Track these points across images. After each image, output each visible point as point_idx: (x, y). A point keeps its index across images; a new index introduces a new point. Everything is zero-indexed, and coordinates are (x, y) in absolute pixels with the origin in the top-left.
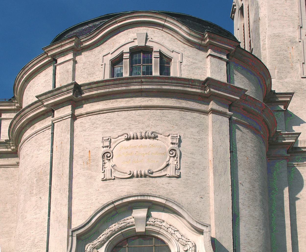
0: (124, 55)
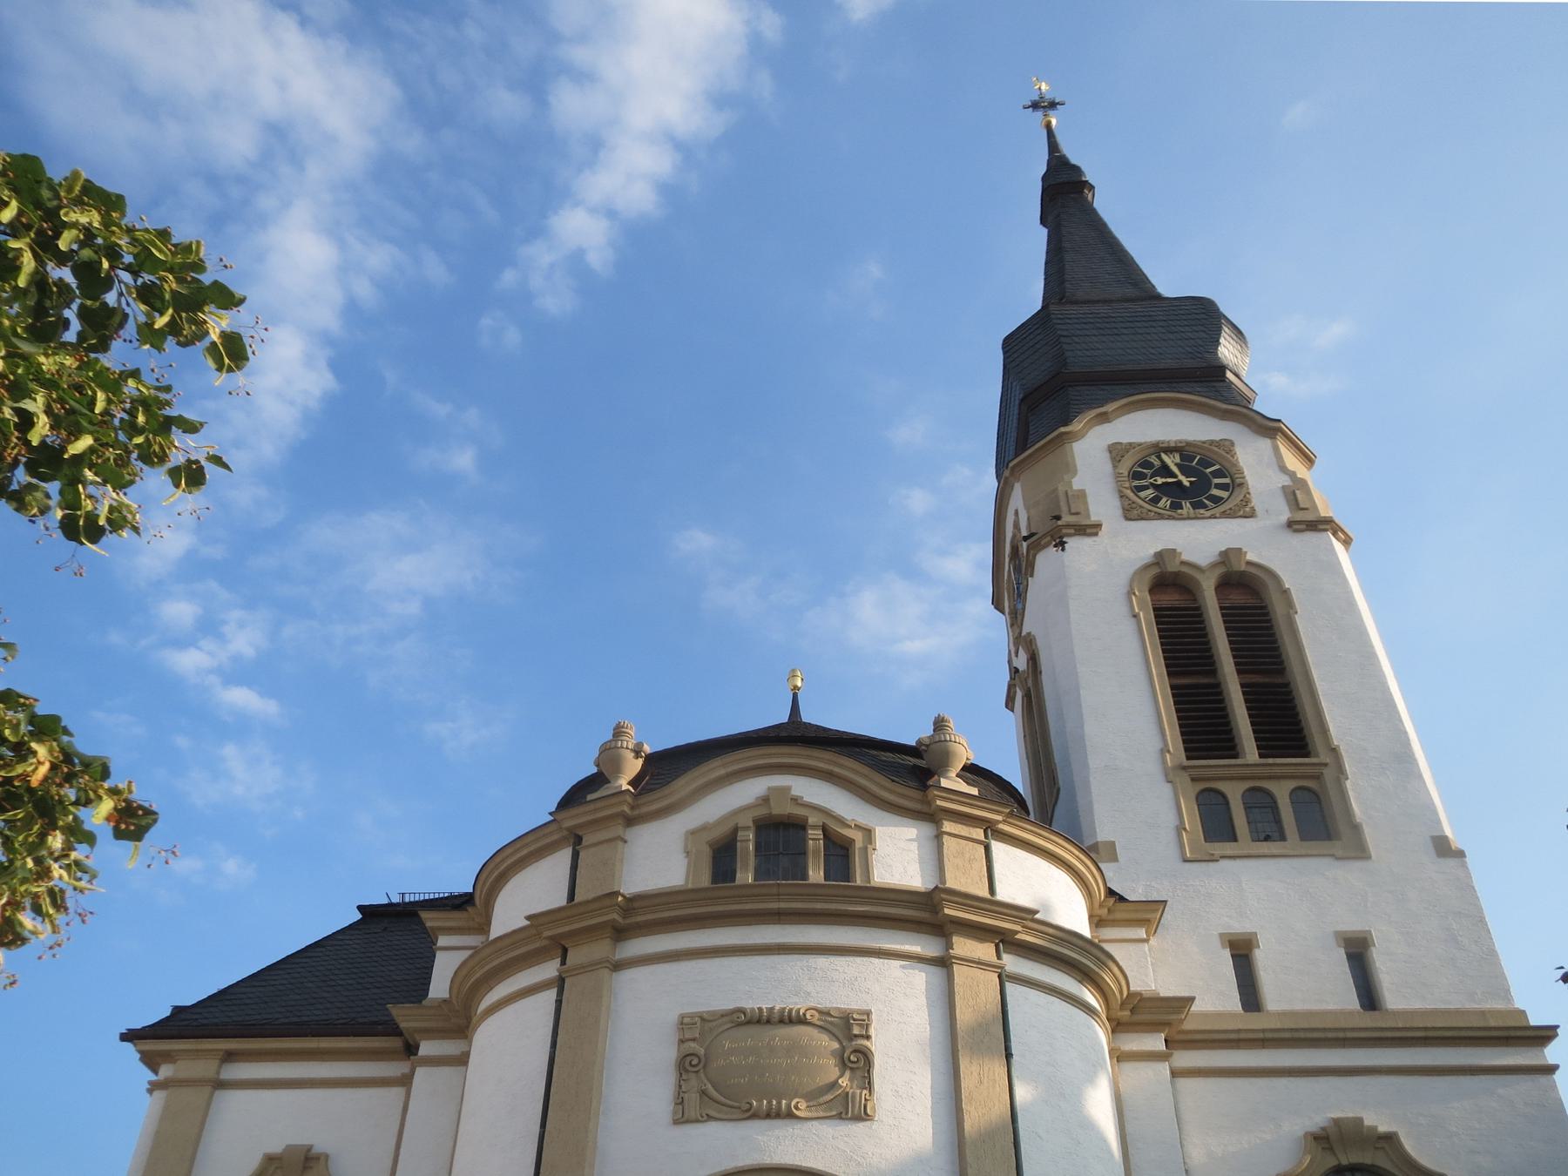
0: (740, 834)
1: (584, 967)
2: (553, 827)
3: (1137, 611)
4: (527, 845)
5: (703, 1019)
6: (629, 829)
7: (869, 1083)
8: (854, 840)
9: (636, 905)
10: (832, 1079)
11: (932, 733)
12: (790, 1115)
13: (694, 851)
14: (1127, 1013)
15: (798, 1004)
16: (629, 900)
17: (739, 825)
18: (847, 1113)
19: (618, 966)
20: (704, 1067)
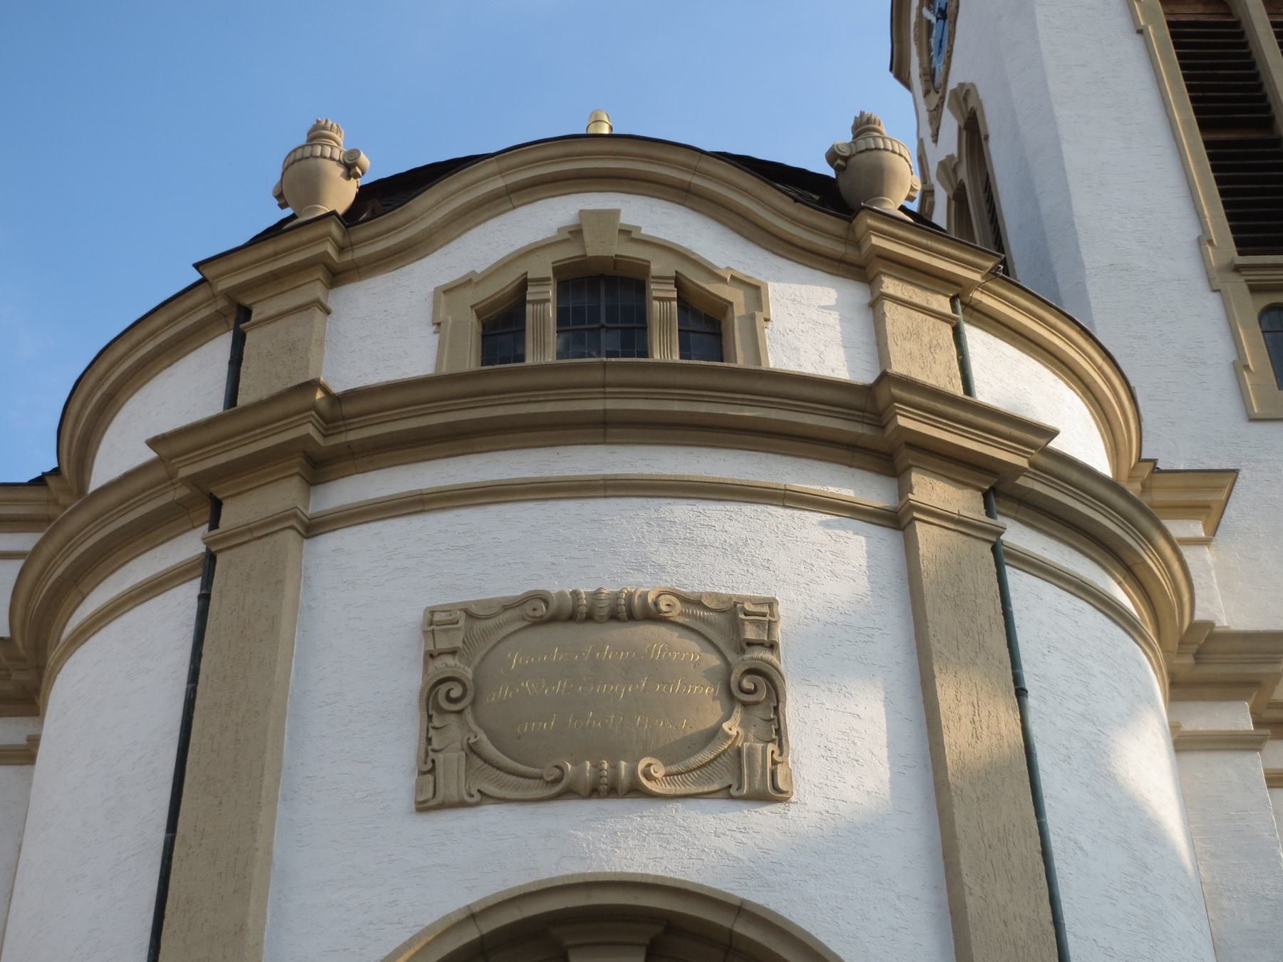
0: (530, 290)
1: (250, 530)
2: (200, 295)
3: (1142, 23)
4: (153, 334)
5: (470, 615)
6: (312, 541)
7: (778, 731)
8: (731, 304)
9: (348, 409)
10: (710, 722)
11: (848, 138)
12: (636, 791)
13: (450, 320)
14: (1189, 660)
15: (643, 584)
16: (336, 400)
17: (529, 276)
18: (740, 788)
19: (313, 528)
20: (474, 703)
